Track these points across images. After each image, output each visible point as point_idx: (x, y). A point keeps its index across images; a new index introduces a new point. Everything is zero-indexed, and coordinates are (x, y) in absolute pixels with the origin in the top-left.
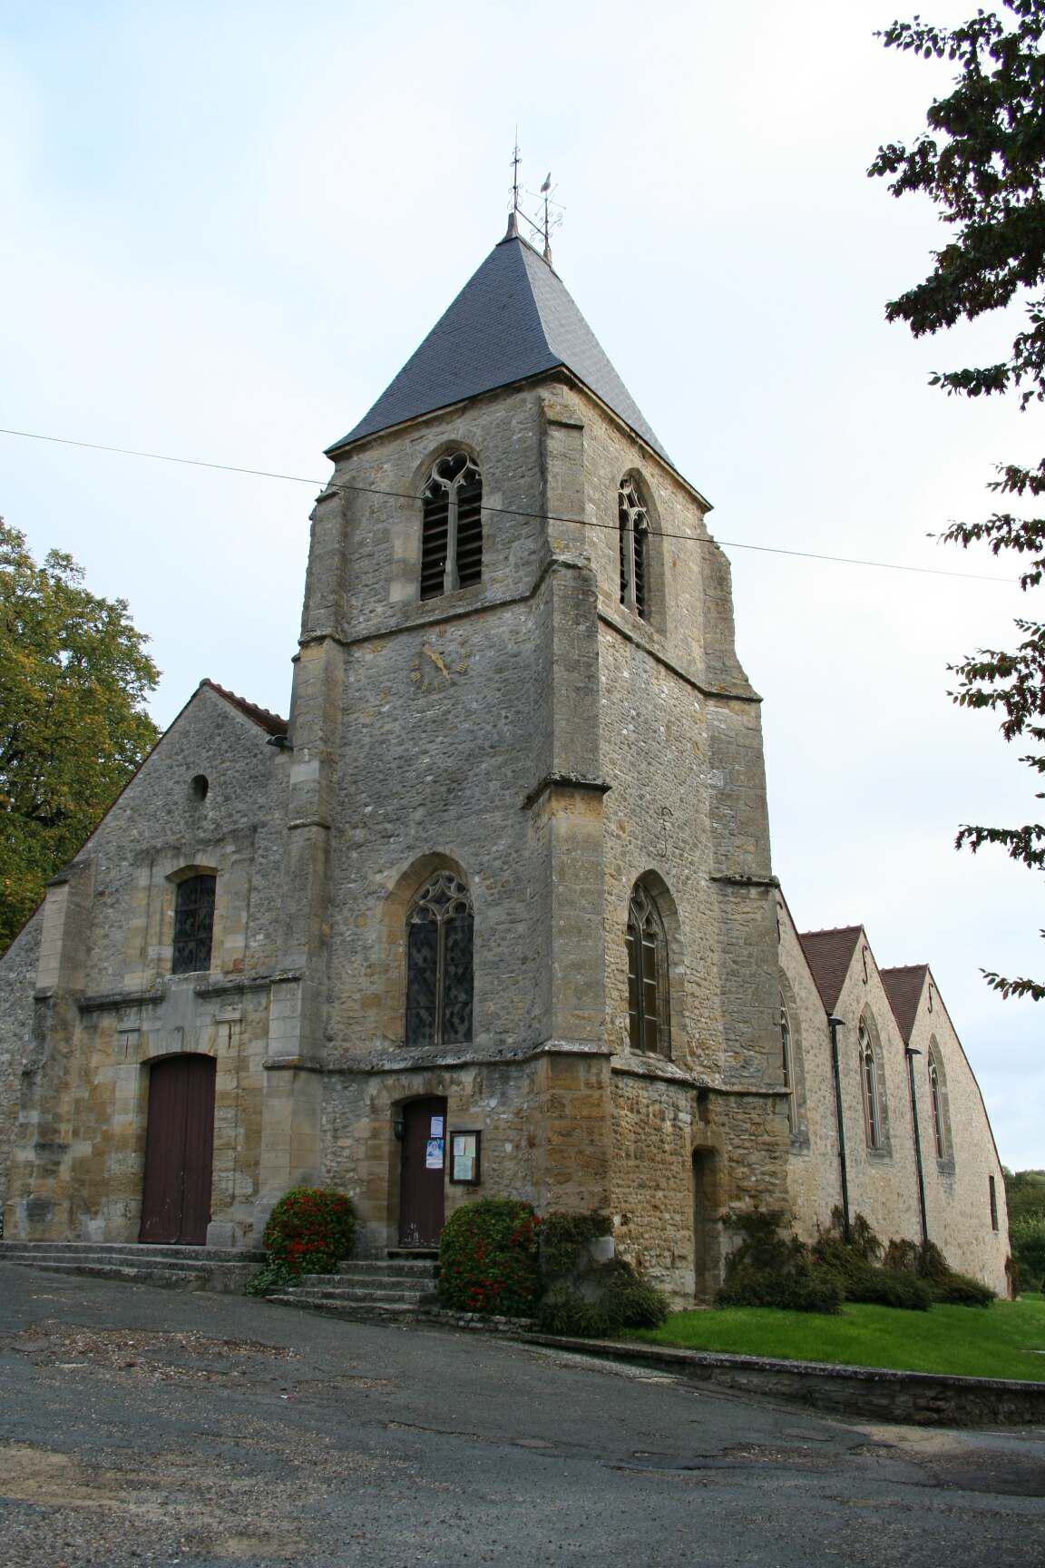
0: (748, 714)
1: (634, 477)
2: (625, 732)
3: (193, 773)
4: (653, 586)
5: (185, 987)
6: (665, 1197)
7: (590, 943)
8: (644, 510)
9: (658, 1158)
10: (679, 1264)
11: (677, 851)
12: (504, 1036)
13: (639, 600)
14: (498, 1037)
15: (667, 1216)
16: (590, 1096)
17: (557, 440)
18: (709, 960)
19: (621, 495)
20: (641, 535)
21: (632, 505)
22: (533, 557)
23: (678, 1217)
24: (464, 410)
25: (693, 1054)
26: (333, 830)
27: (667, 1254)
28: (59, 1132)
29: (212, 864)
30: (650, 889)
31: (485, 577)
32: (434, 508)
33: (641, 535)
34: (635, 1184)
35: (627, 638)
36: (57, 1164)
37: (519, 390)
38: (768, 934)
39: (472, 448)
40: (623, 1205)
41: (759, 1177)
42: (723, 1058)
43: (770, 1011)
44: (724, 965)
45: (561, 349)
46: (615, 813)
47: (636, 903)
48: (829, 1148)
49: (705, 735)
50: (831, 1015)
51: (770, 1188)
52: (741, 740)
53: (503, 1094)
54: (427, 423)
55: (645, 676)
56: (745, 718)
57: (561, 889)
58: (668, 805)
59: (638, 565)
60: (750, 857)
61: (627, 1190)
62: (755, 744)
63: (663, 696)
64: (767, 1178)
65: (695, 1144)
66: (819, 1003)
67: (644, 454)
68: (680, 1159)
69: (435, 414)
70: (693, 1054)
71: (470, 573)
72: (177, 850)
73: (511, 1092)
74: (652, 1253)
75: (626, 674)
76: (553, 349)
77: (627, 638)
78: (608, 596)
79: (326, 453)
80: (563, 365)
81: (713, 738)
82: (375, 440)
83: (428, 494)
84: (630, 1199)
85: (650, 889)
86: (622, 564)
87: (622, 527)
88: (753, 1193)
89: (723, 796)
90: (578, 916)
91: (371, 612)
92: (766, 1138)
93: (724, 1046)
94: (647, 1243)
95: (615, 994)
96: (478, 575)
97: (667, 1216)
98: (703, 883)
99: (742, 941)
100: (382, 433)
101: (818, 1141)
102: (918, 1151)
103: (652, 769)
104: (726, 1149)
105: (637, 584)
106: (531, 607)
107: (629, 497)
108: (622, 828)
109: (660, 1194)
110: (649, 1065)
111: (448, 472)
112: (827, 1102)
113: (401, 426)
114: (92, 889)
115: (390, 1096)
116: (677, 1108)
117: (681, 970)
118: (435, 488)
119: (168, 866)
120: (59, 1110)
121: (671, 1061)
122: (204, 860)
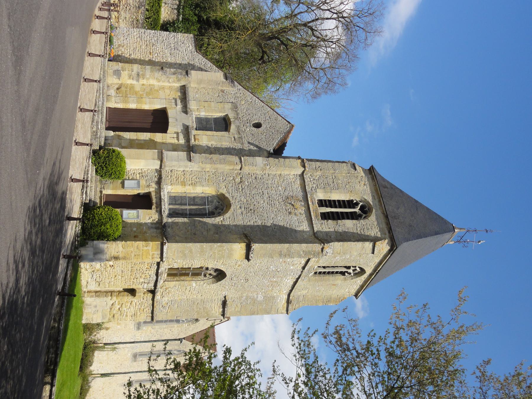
0: (283, 309)
1: (363, 271)
2: (272, 267)
3: (262, 122)
4: (325, 277)
5: (191, 122)
6: (119, 279)
7: (198, 255)
8: (352, 275)
9: (132, 277)
10: (97, 284)
11: (234, 284)
12: (170, 228)
13: (320, 273)
14: (170, 226)
15: (113, 280)
16: (150, 255)
17: (369, 245)
18: (198, 295)
19: (356, 267)
20: (343, 273)
21: (353, 270)
22: (329, 237)
23: (112, 283)
24: (384, 214)
25: (166, 289)
26: (240, 171)
27: (100, 280)
28: (143, 79)
29: (231, 131)
30: (220, 275)
31: (323, 221)
32: (350, 204)
33: (343, 273)
34: (123, 269)
35: (304, 268)
36: (133, 79)
37: (389, 232)
38: (207, 315)
39: (370, 216)
40: (116, 266)
41: (126, 311)
42: (166, 299)
43: (181, 315)
44: (197, 300)
45: (404, 248)
46: (244, 264)
47: (216, 270)
48: (137, 338)
49: (275, 294)
50: (184, 339)
51: (122, 315)
52: (274, 307)
53: (152, 227)
54: (380, 201)
55: (292, 274)
56: (281, 309)
57: (216, 246)
58: (249, 281)
59: (333, 273)
60: (233, 309)
61: (121, 267)
62: (272, 312)
63: (286, 280)
64: (125, 314)
65: (137, 289)
66: (188, 335)
67: (371, 275)
68: (132, 284)
69: (383, 204)
70: (166, 289)
71: (325, 216)
72: (236, 118)
73: (152, 230)
74: (101, 275)
75: (292, 268)
76: (405, 244)
77: (304, 268)
78: (318, 262)
79: (372, 166)
80: (397, 248)
81: (274, 297)
82: (375, 183)
83: (355, 201)
84: (118, 267)
85: (220, 275)
86: (332, 267)
87: (346, 267)
88: (120, 309)
89: (254, 301)
90: (207, 251)
91: (314, 183)
92: (139, 313)
93: (170, 299)
94: (104, 273)
95: (184, 263)
96: (325, 219)
97: (113, 280)
98: (224, 293)
99: (205, 306)
100: (377, 185)
101: (140, 334)
102: (137, 372)
103: (260, 276)
104: (135, 300)
105: (326, 272)
106: (311, 236)
107: (356, 270)
108: (239, 266)
109: (120, 277)
110: (162, 274)
111: (362, 208)
112: (153, 337)
113: (379, 192)
114: (225, 89)
115: (152, 191)
116: (148, 283)
117: (194, 285)
118: (357, 204)
119: (231, 116)
120: (150, 79)
121: (164, 282)
122: (233, 127)
